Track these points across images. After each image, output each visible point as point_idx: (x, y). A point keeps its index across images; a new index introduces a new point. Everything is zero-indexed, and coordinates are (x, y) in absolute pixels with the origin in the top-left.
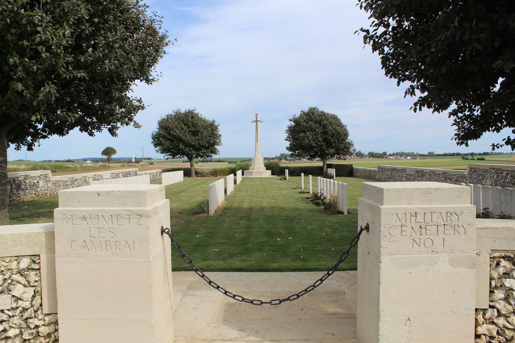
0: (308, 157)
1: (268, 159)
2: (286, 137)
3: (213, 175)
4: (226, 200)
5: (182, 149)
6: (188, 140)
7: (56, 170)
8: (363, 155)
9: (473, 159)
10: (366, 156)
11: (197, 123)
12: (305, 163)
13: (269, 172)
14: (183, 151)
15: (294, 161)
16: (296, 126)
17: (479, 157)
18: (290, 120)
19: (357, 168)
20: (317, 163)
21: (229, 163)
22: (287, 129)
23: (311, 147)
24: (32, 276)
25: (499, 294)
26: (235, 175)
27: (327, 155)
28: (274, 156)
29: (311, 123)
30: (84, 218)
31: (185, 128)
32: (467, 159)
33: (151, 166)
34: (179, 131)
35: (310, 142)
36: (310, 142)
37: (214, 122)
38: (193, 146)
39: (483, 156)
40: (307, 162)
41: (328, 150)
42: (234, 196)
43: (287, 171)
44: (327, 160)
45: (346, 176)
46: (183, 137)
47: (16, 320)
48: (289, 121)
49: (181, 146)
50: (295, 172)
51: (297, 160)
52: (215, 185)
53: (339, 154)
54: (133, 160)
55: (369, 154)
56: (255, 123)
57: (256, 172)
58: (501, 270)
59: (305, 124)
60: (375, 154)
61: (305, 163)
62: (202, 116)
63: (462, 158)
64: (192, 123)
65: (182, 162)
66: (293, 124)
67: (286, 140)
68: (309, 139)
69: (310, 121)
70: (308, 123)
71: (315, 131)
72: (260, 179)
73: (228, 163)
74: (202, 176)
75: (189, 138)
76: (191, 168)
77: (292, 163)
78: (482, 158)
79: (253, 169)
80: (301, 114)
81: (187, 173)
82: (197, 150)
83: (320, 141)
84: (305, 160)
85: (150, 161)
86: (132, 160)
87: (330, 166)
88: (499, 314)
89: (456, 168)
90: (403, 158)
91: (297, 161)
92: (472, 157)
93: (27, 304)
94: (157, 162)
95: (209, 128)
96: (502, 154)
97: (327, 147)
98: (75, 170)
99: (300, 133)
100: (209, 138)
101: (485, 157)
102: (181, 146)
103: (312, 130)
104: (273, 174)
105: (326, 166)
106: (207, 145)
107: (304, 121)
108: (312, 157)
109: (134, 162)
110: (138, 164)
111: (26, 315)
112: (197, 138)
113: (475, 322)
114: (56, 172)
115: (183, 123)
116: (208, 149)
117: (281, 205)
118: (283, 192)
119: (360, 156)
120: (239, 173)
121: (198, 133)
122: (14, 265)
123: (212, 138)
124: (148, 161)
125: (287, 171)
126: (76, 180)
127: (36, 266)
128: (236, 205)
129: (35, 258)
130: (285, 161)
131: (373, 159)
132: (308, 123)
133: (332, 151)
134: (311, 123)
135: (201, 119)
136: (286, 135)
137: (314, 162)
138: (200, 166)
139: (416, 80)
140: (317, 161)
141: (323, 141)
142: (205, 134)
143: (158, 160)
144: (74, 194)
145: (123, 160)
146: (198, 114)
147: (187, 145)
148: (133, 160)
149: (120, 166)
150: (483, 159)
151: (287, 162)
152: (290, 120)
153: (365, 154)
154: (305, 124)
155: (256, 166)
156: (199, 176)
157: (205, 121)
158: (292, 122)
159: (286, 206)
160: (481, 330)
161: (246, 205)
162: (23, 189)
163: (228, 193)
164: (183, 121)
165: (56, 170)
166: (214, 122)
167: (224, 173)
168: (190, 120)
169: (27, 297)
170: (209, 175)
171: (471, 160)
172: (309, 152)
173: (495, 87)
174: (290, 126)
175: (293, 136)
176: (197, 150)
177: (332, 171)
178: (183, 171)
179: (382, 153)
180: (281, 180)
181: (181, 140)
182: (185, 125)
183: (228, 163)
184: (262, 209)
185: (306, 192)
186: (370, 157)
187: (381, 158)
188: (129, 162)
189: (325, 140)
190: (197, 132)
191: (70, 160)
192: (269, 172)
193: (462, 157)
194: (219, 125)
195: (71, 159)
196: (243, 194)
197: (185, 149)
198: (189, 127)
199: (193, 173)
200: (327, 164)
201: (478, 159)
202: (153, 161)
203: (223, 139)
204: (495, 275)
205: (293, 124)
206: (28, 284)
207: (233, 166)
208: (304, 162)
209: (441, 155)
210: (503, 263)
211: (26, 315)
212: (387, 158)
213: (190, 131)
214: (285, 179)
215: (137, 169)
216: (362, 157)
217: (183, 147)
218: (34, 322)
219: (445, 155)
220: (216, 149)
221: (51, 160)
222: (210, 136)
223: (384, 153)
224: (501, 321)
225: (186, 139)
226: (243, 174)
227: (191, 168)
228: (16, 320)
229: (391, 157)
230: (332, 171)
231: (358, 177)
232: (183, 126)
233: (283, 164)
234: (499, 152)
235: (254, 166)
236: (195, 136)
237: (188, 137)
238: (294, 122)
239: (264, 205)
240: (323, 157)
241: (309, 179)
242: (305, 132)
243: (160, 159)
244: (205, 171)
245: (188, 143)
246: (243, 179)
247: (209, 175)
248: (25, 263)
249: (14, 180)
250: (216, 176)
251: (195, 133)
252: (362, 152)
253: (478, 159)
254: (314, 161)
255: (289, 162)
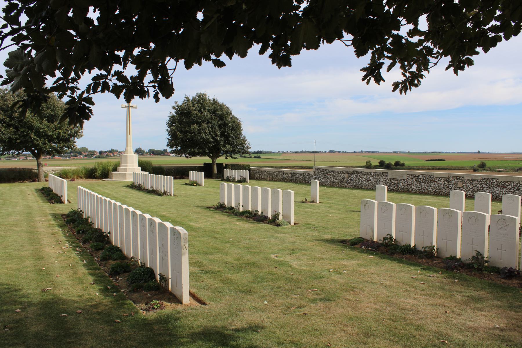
8: (144, 152)
9: (251, 157)
10: (147, 153)
11: (54, 103)
15: (70, 157)
17: (256, 155)
40: (84, 159)
51: (73, 156)
55: (150, 151)
60: (156, 151)
63: (240, 156)
77: (67, 160)
78: (258, 156)
80: (185, 100)
84: (82, 157)
91: (73, 157)
92: (250, 155)
113: (182, 266)
119: (140, 153)
130: (59, 158)
131: (154, 156)
137: (92, 159)
139: (69, 31)
140: (95, 157)
141: (221, 136)
150: (259, 157)
151: (61, 158)
153: (145, 151)
169: (320, 225)
171: (249, 157)
173: (118, 52)
179: (162, 150)
185: (148, 187)
186: (150, 154)
187: (162, 155)
189: (223, 134)
193: (241, 155)
208: (81, 159)
209: (351, 153)
212: (167, 155)
216: (142, 154)
219: (302, 152)
223: (164, 150)
229: (172, 155)
252: (143, 149)
253: (255, 157)
254: (92, 158)
255: (64, 158)
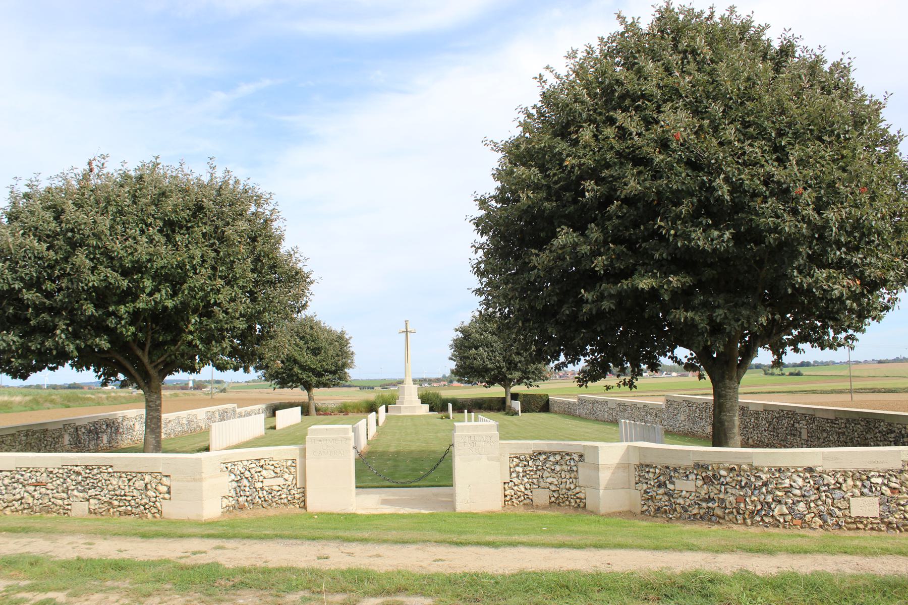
0: (484, 384)
1: (430, 381)
2: (450, 355)
3: (341, 412)
4: (368, 444)
5: (297, 375)
6: (306, 361)
7: (70, 404)
9: (783, 374)
12: (479, 391)
13: (426, 407)
14: (298, 377)
16: (464, 338)
17: (792, 370)
18: (457, 330)
19: (554, 400)
20: (497, 391)
21: (361, 388)
22: (452, 342)
23: (487, 370)
24: (292, 469)
25: (514, 475)
26: (377, 412)
27: (511, 380)
28: (440, 376)
29: (485, 334)
30: (320, 441)
31: (302, 343)
32: (772, 374)
33: (222, 395)
34: (293, 348)
35: (484, 362)
36: (484, 362)
37: (343, 333)
38: (313, 370)
39: (798, 369)
41: (511, 374)
42: (377, 440)
43: (450, 405)
44: (511, 387)
45: (539, 412)
46: (298, 358)
47: (285, 490)
48: (454, 331)
49: (295, 369)
50: (460, 406)
52: (358, 426)
53: (528, 378)
54: (191, 384)
56: (404, 335)
57: (406, 408)
58: (514, 463)
59: (477, 336)
61: (479, 391)
62: (326, 325)
64: (312, 335)
65: (298, 394)
66: (461, 335)
67: (451, 359)
68: (482, 359)
69: (485, 331)
70: (481, 334)
71: (492, 346)
72: (412, 417)
73: (358, 389)
74: (325, 414)
75: (306, 358)
76: (309, 403)
79: (402, 403)
81: (305, 411)
82: (319, 375)
83: (499, 362)
85: (222, 386)
86: (188, 384)
87: (515, 397)
88: (515, 485)
89: (788, 390)
90: (664, 375)
93: (290, 483)
94: (233, 388)
95: (336, 343)
96: (834, 363)
97: (508, 369)
98: (99, 404)
99: (470, 348)
100: (336, 358)
101: (802, 370)
102: (296, 369)
103: (488, 344)
104: (431, 409)
105: (509, 397)
106: (334, 368)
107: (476, 332)
108: (491, 383)
109: (191, 388)
110: (198, 392)
111: (289, 488)
112: (319, 357)
114: (69, 407)
115: (297, 335)
116: (334, 374)
117: (433, 449)
118: (439, 435)
120: (382, 409)
121: (321, 351)
122: (284, 464)
123: (340, 358)
124: (216, 385)
125: (450, 405)
126: (170, 421)
127: (294, 465)
128: (380, 449)
129: (294, 461)
132: (481, 334)
133: (517, 374)
134: (485, 334)
135: (324, 330)
136: (450, 352)
138: (323, 396)
142: (331, 352)
143: (235, 385)
144: (315, 430)
145: (171, 385)
146: (320, 322)
147: (303, 368)
148: (191, 384)
149: (171, 395)
150: (798, 374)
152: (457, 330)
154: (477, 336)
155: (407, 398)
156: (321, 415)
157: (330, 332)
158: (459, 333)
159: (438, 449)
160: (507, 493)
161: (392, 449)
162: (120, 434)
163: (370, 437)
164: (298, 334)
165: (70, 404)
166: (343, 333)
167: (358, 409)
168: (308, 331)
170: (336, 413)
172: (483, 377)
174: (455, 338)
175: (460, 354)
176: (319, 375)
177: (517, 405)
178: (299, 408)
180: (442, 418)
181: (295, 362)
182: (302, 338)
183: (358, 389)
184: (411, 452)
188: (183, 388)
190: (319, 349)
191: (75, 384)
192: (426, 407)
193: (765, 371)
194: (351, 338)
195: (77, 382)
196: (389, 438)
197: (301, 374)
198: (306, 343)
199: (313, 410)
200: (512, 394)
201: (791, 374)
202: (225, 386)
203: (357, 359)
204: (512, 466)
205: (461, 335)
206: (290, 473)
207: (371, 396)
210: (515, 459)
211: (289, 488)
213: (308, 348)
214: (448, 417)
215: (235, 405)
217: (299, 372)
218: (293, 492)
220: (345, 373)
221: (40, 383)
222: (338, 356)
224: (516, 488)
225: (303, 360)
226: (387, 411)
227: (309, 403)
228: (285, 490)
230: (517, 405)
231: (556, 413)
232: (298, 340)
233: (446, 393)
234: (828, 360)
235: (404, 398)
236: (316, 355)
237: (306, 357)
238: (462, 332)
239: (413, 448)
240: (504, 381)
241: (471, 416)
242: (476, 348)
243: (238, 382)
244: (330, 406)
245: (306, 366)
246: (387, 418)
247: (336, 413)
248: (290, 463)
249: (113, 423)
250: (347, 414)
251: (316, 351)
253: (791, 374)
